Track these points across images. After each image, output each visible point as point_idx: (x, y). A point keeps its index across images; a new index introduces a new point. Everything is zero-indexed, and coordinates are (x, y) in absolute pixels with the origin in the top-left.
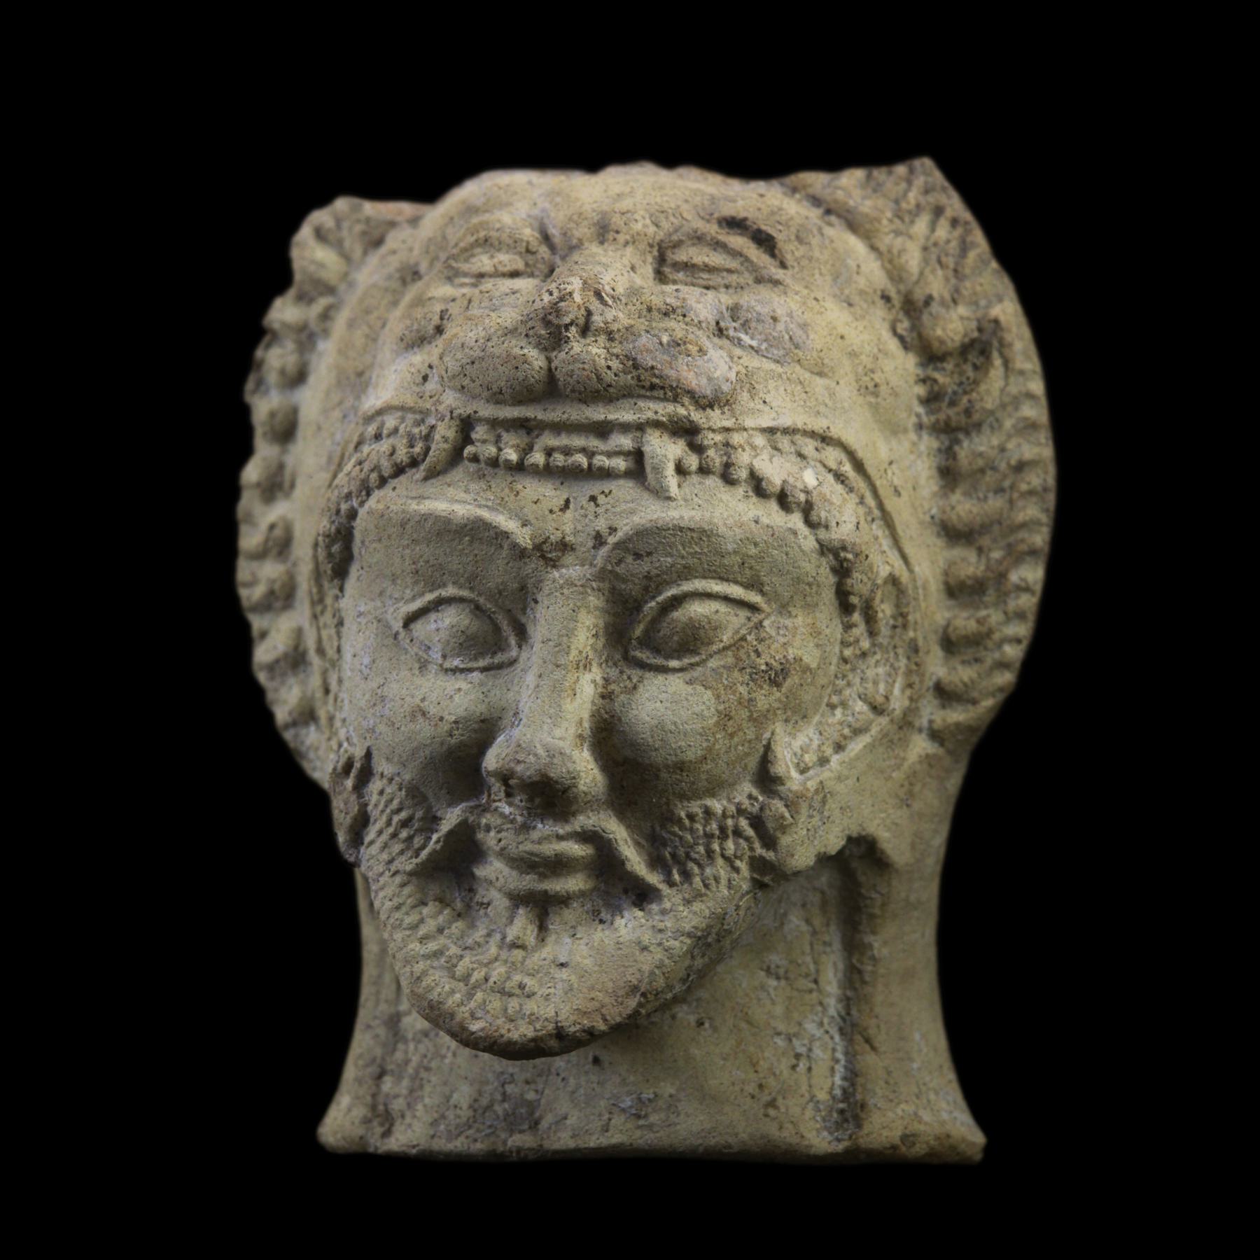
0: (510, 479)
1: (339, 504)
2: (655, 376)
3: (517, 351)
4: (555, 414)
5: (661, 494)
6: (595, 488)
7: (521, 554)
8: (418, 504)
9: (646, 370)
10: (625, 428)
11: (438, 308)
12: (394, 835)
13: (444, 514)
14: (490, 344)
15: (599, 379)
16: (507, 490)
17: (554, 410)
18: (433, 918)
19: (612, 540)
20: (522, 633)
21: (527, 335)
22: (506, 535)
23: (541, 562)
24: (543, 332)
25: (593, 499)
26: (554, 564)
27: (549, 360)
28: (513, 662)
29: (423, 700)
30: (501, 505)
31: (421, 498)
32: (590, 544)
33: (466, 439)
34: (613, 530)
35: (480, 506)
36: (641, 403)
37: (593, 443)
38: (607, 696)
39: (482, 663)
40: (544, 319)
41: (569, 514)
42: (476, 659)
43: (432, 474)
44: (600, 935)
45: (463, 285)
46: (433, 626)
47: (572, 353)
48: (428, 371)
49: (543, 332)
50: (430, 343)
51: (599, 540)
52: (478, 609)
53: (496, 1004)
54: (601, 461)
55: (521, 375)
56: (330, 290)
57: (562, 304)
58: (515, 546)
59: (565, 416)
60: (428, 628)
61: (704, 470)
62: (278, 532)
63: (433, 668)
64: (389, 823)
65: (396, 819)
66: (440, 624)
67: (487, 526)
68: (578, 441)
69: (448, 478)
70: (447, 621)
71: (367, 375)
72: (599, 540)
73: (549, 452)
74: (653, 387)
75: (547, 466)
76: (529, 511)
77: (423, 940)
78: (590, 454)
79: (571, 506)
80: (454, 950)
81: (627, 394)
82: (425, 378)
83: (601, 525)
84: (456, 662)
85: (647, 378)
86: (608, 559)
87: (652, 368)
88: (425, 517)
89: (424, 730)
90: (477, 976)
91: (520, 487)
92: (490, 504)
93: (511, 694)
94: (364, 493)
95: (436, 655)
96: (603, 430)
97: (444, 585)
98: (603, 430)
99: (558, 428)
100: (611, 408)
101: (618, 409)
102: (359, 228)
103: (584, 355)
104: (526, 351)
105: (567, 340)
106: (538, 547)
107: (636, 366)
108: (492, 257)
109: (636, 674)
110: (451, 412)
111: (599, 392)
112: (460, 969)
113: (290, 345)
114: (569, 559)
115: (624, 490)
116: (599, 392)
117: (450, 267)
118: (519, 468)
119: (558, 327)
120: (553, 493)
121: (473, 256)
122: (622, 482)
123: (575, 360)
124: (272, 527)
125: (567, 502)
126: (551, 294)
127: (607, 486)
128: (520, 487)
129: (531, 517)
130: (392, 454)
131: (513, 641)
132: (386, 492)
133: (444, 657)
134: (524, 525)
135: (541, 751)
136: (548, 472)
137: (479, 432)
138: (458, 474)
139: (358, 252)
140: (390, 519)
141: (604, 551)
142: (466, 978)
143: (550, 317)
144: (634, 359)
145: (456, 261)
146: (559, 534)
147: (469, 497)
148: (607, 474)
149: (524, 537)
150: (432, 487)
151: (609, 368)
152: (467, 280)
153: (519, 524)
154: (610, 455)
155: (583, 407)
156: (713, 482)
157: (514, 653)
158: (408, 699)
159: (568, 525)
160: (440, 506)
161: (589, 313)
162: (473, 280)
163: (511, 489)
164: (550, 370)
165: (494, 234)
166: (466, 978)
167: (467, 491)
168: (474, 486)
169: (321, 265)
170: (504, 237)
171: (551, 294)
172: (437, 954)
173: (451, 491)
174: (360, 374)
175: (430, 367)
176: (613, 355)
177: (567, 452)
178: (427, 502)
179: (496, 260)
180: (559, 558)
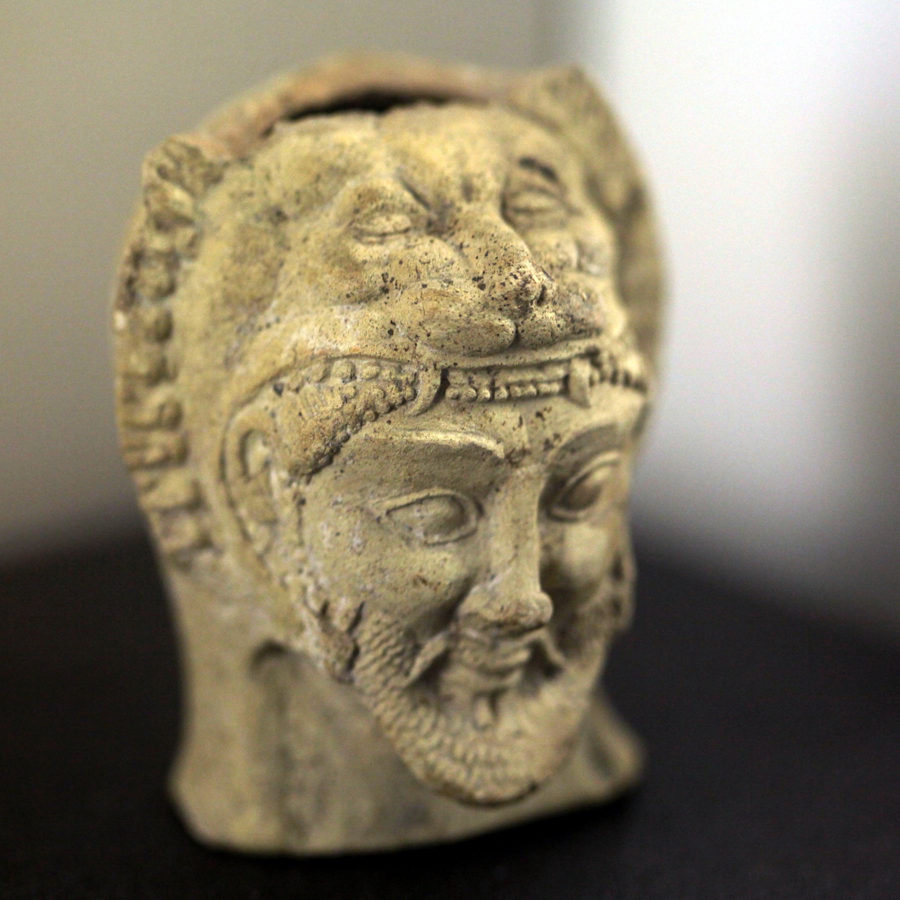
0: (483, 409)
1: (335, 433)
2: (583, 324)
3: (497, 323)
4: (516, 360)
5: (583, 404)
6: (539, 406)
7: (497, 462)
8: (417, 435)
9: (578, 322)
10: (558, 362)
11: (378, 272)
12: (389, 663)
13: (444, 443)
14: (472, 318)
15: (552, 334)
16: (483, 418)
17: (513, 357)
18: (426, 718)
19: (558, 444)
20: (481, 511)
21: (500, 309)
22: (490, 453)
23: (509, 466)
24: (516, 307)
25: (539, 415)
26: (515, 465)
27: (517, 326)
28: (474, 532)
29: (421, 570)
30: (481, 430)
31: (418, 430)
32: (542, 448)
33: (445, 383)
34: (557, 436)
35: (466, 433)
36: (571, 344)
37: (540, 376)
38: (546, 548)
39: (455, 535)
40: (516, 298)
41: (524, 428)
42: (448, 533)
43: (425, 410)
44: (534, 707)
45: (371, 243)
46: (418, 515)
47: (536, 320)
48: (392, 327)
49: (516, 307)
50: (376, 299)
51: (548, 445)
52: (453, 500)
53: (488, 774)
54: (545, 388)
55: (500, 339)
56: (186, 221)
57: (528, 286)
58: (496, 458)
59: (522, 361)
60: (411, 515)
61: (602, 379)
62: (168, 412)
63: (416, 544)
64: (384, 654)
65: (391, 652)
66: (425, 514)
67: (475, 448)
68: (529, 376)
69: (436, 412)
70: (432, 512)
71: (266, 301)
72: (548, 445)
73: (508, 387)
74: (581, 331)
75: (510, 396)
76: (500, 432)
77: (427, 736)
78: (535, 383)
79: (524, 421)
80: (448, 741)
81: (566, 338)
82: (391, 332)
83: (549, 433)
84: (436, 538)
85: (579, 327)
86: (556, 458)
87: (583, 320)
88: (429, 446)
89: (427, 593)
90: (470, 757)
91: (490, 414)
92: (473, 430)
93: (481, 557)
94: (358, 425)
95: (419, 533)
96: (541, 366)
97: (431, 487)
98: (541, 366)
99: (510, 369)
100: (551, 350)
101: (556, 350)
102: (200, 171)
103: (544, 321)
104: (503, 322)
105: (531, 311)
106: (508, 457)
107: (573, 321)
108: (388, 219)
109: (558, 527)
110: (435, 365)
111: (552, 340)
112: (459, 751)
113: (161, 267)
114: (527, 460)
115: (559, 406)
116: (552, 340)
117: (356, 228)
118: (492, 400)
119: (527, 302)
120: (512, 414)
121: (373, 218)
122: (555, 399)
123: (539, 324)
124: (162, 407)
125: (521, 419)
126: (516, 277)
127: (549, 403)
128: (490, 414)
129: (503, 436)
130: (384, 397)
131: (473, 517)
132: (381, 424)
133: (426, 534)
134: (498, 442)
135: (535, 606)
136: (511, 400)
137: (457, 378)
138: (442, 409)
139: (199, 186)
140: (394, 446)
141: (552, 453)
142: (463, 759)
143: (521, 297)
144: (572, 316)
145: (361, 223)
146: (520, 444)
147: (457, 427)
148: (541, 396)
149: (499, 451)
150: (423, 422)
151: (559, 326)
152: (374, 239)
153: (495, 441)
154: (549, 382)
155: (533, 352)
156: (606, 386)
157: (473, 523)
158: (407, 571)
159: (522, 437)
160: (438, 437)
161: (544, 288)
162: (379, 239)
163: (485, 416)
164: (517, 332)
165: (388, 201)
166: (463, 759)
167: (455, 422)
168: (459, 418)
169: (181, 204)
170: (397, 203)
171: (516, 277)
172: (440, 745)
173: (443, 423)
174: (259, 300)
175: (393, 323)
176: (559, 315)
177: (521, 384)
178: (425, 433)
179: (392, 222)
180: (520, 461)
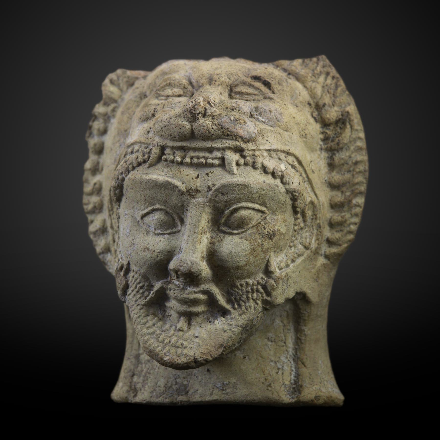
0: (178, 167)
1: (118, 176)
2: (229, 131)
3: (181, 123)
4: (194, 144)
5: (231, 172)
6: (208, 170)
7: (182, 193)
8: (146, 176)
9: (226, 129)
10: (218, 149)
11: (153, 107)
12: (138, 292)
13: (155, 179)
14: (171, 120)
15: (209, 132)
16: (177, 171)
17: (193, 143)
18: (151, 321)
19: (214, 189)
20: (182, 221)
21: (184, 117)
22: (177, 187)
23: (189, 196)
24: (190, 116)
25: (207, 174)
26: (193, 197)
27: (192, 126)
28: (179, 231)
29: (148, 244)
30: (175, 176)
31: (147, 174)
32: (206, 190)
33: (163, 153)
34: (214, 185)
35: (167, 177)
36: (224, 141)
37: (207, 155)
38: (212, 243)
39: (168, 232)
40: (190, 111)
41: (199, 180)
42: (166, 230)
43: (151, 166)
44: (210, 326)
45: (162, 99)
46: (151, 219)
47: (200, 123)
48: (150, 129)
49: (190, 116)
50: (150, 120)
51: (209, 189)
52: (167, 213)
53: (173, 350)
54: (210, 161)
55: (182, 131)
56: (115, 101)
57: (196, 106)
58: (180, 191)
59: (197, 145)
60: (150, 219)
61: (246, 164)
62: (97, 186)
63: (151, 233)
64: (136, 287)
65: (138, 286)
66: (154, 218)
67: (170, 184)
68: (202, 154)
69: (156, 167)
70: (156, 217)
71: (128, 131)
72: (209, 189)
73: (192, 158)
74: (228, 135)
75: (191, 163)
76: (185, 179)
77: (148, 328)
78: (206, 159)
79: (200, 177)
80: (158, 332)
81: (219, 137)
82: (148, 132)
83: (210, 183)
84: (159, 231)
85: (226, 132)
86: (212, 195)
87: (228, 128)
88: (149, 181)
89: (148, 255)
90: (167, 341)
91: (181, 170)
92: (171, 176)
93: (178, 242)
94: (127, 172)
95: (152, 229)
96: (210, 150)
97: (155, 204)
98: (210, 150)
99: (195, 149)
100: (213, 142)
101: (216, 143)
102: (125, 80)
103: (204, 124)
104: (184, 122)
105: (198, 119)
106: (188, 191)
107: (222, 128)
109: (222, 235)
110: (158, 144)
111: (209, 137)
112: (161, 338)
113: (101, 121)
114: (199, 195)
115: (218, 171)
116: (209, 137)
117: (157, 93)
118: (181, 163)
119: (195, 114)
120: (193, 172)
121: (165, 89)
122: (217, 168)
123: (201, 126)
124: (95, 184)
125: (198, 175)
126: (192, 103)
127: (212, 170)
128: (181, 170)
129: (185, 181)
130: (137, 159)
131: (179, 224)
132: (135, 172)
133: (155, 229)
134: (183, 183)
135: (189, 262)
136: (191, 165)
137: (167, 151)
138: (160, 165)
139: (125, 88)
140: (136, 181)
141: (211, 192)
142: (163, 342)
143: (192, 111)
144: (221, 125)
145: (159, 91)
146: (195, 186)
147: (164, 174)
148: (212, 166)
149: (183, 188)
150: (151, 170)
151: (213, 128)
152: (163, 98)
153: (181, 183)
154: (213, 159)
155: (204, 142)
156: (249, 168)
157: (179, 228)
158: (143, 244)
159: (198, 183)
160: (153, 177)
161: (206, 109)
162: (165, 98)
163: (179, 171)
164: (192, 129)
165: (172, 82)
166: (163, 342)
167: (163, 171)
168: (165, 170)
169: (112, 93)
170: (176, 83)
171: (192, 103)
172: (153, 333)
173: (157, 172)
174: (126, 131)
175: (150, 128)
176: (214, 124)
177: (198, 158)
178: (149, 175)
179: (173, 91)
180: (195, 195)
